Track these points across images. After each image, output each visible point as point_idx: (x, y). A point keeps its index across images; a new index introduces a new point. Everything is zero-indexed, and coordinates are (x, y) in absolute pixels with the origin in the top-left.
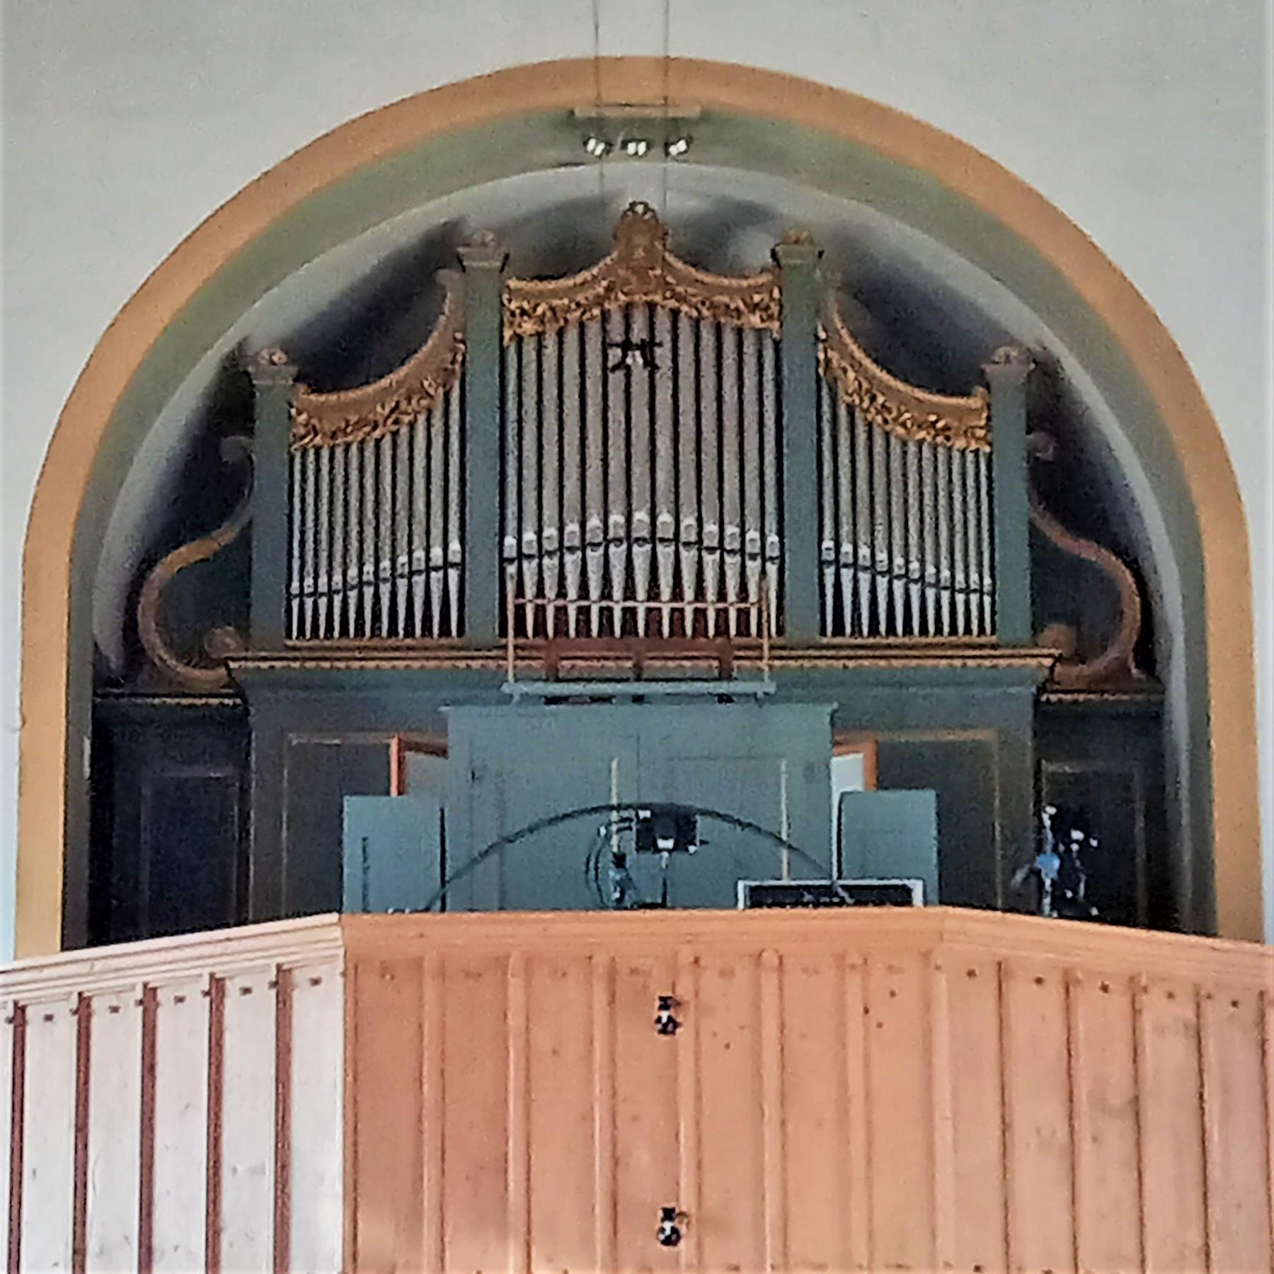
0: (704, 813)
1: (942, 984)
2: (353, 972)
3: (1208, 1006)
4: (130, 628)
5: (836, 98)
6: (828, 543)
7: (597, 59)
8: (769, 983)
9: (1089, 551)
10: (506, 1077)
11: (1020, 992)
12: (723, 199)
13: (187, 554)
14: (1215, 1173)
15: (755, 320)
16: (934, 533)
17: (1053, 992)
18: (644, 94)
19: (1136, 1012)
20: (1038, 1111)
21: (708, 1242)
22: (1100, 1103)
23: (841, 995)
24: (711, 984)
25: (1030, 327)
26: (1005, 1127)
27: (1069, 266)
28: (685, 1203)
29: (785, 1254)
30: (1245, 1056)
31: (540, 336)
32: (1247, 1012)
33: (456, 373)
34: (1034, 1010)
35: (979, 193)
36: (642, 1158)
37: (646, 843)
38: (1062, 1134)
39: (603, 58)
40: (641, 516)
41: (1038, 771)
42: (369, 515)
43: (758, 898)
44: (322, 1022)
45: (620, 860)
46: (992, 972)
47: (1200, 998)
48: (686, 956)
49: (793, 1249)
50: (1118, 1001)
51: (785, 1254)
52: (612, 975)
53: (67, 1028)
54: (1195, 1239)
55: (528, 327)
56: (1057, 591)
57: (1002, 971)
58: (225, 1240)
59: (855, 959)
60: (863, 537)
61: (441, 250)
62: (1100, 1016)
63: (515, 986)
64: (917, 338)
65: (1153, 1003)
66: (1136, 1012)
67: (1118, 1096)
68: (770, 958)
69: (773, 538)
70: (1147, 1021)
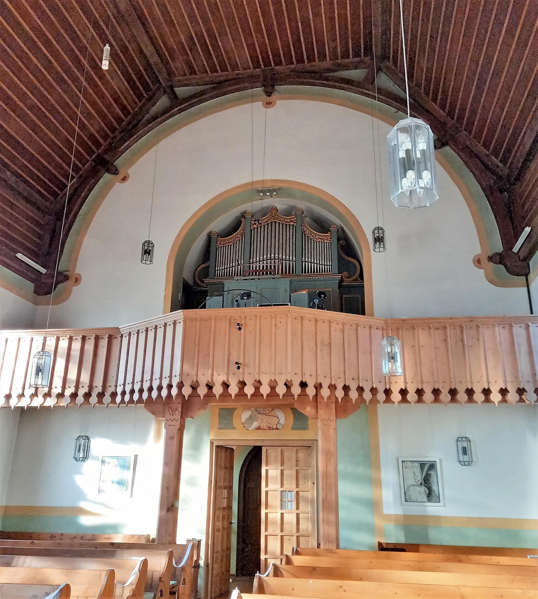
0: (254, 292)
1: (289, 320)
2: (185, 321)
3: (345, 326)
4: (194, 279)
5: (300, 184)
6: (303, 258)
7: (263, 180)
8: (258, 321)
9: (350, 259)
10: (240, 349)
11: (305, 322)
12: (288, 205)
13: (204, 265)
14: (346, 357)
15: (292, 223)
16: (322, 258)
17: (313, 323)
18: (268, 185)
19: (330, 326)
20: (309, 344)
21: (245, 369)
22: (322, 343)
23: (271, 323)
24: (248, 321)
25: (338, 222)
26: (302, 347)
27: (336, 205)
28: (241, 361)
29: (259, 371)
30: (354, 337)
31: (257, 227)
32: (354, 327)
33: (243, 235)
34: (309, 326)
35: (324, 197)
36: (234, 353)
37: (242, 298)
38: (314, 349)
39: (266, 180)
40: (273, 255)
41: (341, 299)
42: (228, 258)
43: (260, 306)
44: (180, 328)
45: (237, 301)
46: (300, 318)
47: (344, 324)
48: (243, 317)
49: (261, 370)
50: (326, 325)
51: (259, 371)
52: (230, 320)
53: (145, 332)
54: (342, 369)
55: (255, 226)
56: (343, 266)
57: (302, 318)
58: (164, 369)
59: (273, 316)
60: (310, 257)
61: (243, 215)
62: (323, 327)
63: (213, 322)
64: (322, 226)
65: (334, 325)
66: (330, 326)
67: (326, 341)
68: (258, 316)
69: (294, 258)
70: (332, 329)
